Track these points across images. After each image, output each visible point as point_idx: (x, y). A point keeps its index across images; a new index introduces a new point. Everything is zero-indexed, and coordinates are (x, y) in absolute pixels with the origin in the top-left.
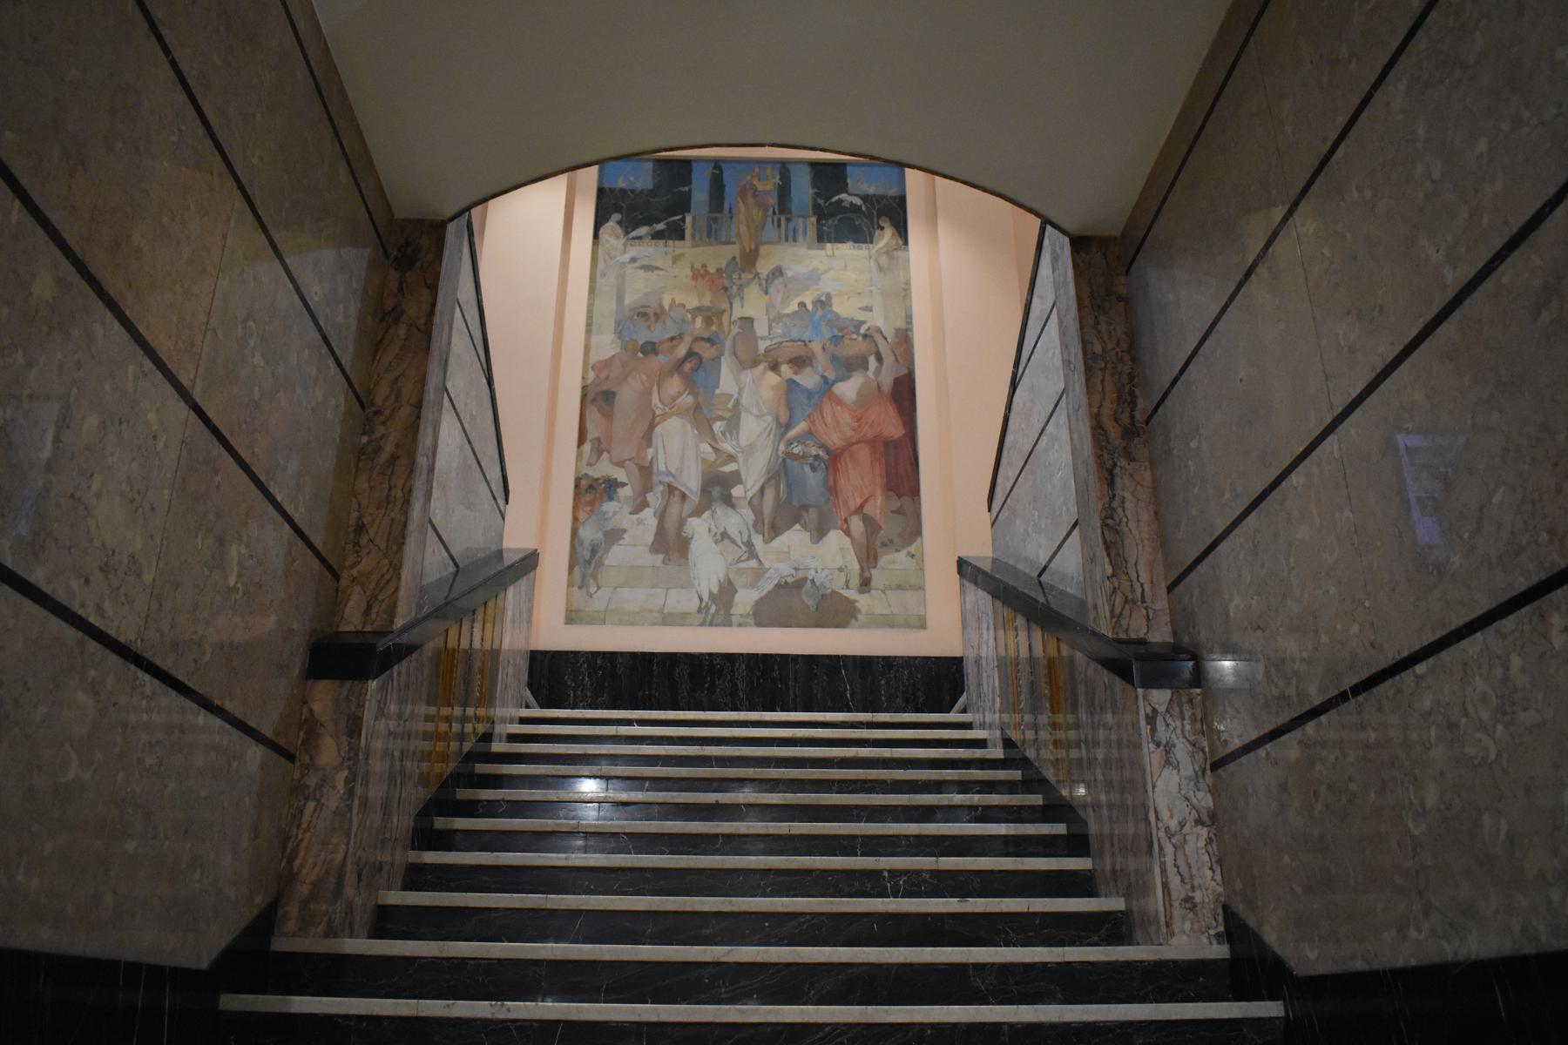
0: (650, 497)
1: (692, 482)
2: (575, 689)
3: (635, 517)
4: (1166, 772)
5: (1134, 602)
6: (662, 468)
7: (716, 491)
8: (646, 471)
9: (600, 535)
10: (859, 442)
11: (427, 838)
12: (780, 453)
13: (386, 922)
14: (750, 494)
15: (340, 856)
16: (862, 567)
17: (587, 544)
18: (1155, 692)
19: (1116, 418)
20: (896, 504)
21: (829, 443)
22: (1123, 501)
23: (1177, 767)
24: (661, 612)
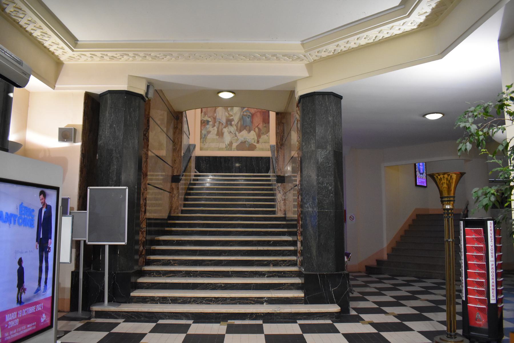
0: (216, 124)
1: (224, 121)
2: (202, 164)
3: (213, 128)
4: (279, 194)
5: (279, 170)
6: (218, 118)
7: (229, 123)
8: (215, 119)
9: (206, 132)
10: (258, 112)
11: (186, 200)
12: (242, 114)
13: (183, 212)
14: (235, 123)
15: (178, 205)
16: (257, 139)
17: (203, 134)
18: (279, 184)
19: (280, 143)
20: (265, 125)
21: (251, 112)
22: (279, 155)
23: (281, 193)
24: (218, 148)
